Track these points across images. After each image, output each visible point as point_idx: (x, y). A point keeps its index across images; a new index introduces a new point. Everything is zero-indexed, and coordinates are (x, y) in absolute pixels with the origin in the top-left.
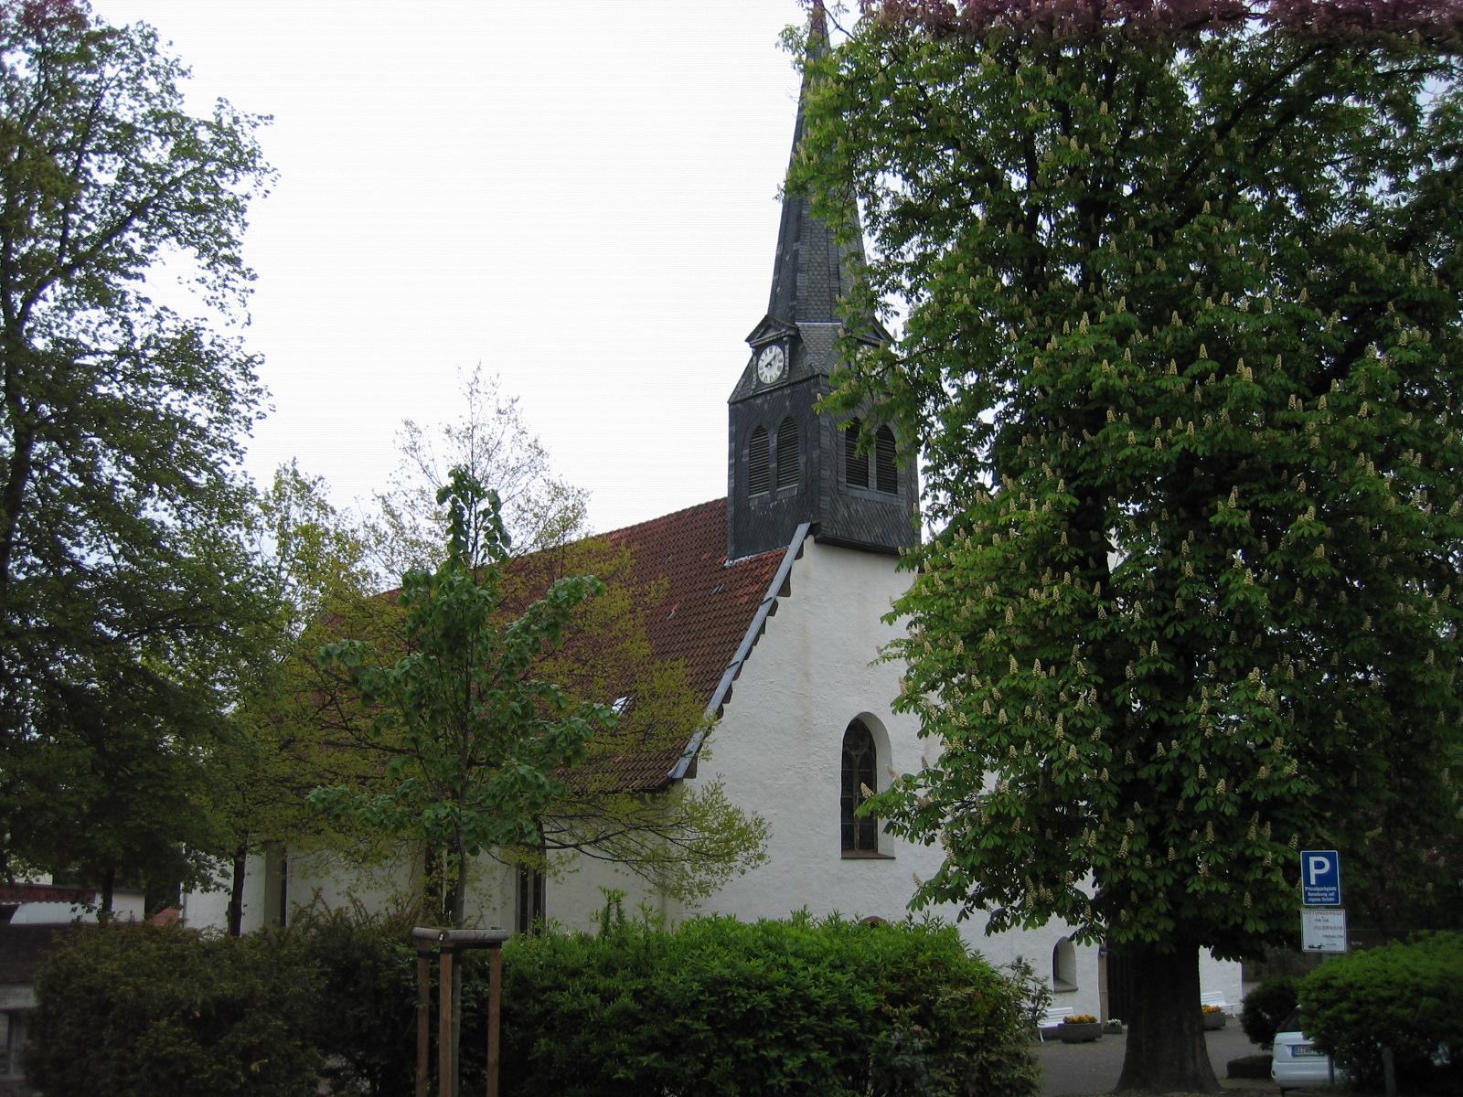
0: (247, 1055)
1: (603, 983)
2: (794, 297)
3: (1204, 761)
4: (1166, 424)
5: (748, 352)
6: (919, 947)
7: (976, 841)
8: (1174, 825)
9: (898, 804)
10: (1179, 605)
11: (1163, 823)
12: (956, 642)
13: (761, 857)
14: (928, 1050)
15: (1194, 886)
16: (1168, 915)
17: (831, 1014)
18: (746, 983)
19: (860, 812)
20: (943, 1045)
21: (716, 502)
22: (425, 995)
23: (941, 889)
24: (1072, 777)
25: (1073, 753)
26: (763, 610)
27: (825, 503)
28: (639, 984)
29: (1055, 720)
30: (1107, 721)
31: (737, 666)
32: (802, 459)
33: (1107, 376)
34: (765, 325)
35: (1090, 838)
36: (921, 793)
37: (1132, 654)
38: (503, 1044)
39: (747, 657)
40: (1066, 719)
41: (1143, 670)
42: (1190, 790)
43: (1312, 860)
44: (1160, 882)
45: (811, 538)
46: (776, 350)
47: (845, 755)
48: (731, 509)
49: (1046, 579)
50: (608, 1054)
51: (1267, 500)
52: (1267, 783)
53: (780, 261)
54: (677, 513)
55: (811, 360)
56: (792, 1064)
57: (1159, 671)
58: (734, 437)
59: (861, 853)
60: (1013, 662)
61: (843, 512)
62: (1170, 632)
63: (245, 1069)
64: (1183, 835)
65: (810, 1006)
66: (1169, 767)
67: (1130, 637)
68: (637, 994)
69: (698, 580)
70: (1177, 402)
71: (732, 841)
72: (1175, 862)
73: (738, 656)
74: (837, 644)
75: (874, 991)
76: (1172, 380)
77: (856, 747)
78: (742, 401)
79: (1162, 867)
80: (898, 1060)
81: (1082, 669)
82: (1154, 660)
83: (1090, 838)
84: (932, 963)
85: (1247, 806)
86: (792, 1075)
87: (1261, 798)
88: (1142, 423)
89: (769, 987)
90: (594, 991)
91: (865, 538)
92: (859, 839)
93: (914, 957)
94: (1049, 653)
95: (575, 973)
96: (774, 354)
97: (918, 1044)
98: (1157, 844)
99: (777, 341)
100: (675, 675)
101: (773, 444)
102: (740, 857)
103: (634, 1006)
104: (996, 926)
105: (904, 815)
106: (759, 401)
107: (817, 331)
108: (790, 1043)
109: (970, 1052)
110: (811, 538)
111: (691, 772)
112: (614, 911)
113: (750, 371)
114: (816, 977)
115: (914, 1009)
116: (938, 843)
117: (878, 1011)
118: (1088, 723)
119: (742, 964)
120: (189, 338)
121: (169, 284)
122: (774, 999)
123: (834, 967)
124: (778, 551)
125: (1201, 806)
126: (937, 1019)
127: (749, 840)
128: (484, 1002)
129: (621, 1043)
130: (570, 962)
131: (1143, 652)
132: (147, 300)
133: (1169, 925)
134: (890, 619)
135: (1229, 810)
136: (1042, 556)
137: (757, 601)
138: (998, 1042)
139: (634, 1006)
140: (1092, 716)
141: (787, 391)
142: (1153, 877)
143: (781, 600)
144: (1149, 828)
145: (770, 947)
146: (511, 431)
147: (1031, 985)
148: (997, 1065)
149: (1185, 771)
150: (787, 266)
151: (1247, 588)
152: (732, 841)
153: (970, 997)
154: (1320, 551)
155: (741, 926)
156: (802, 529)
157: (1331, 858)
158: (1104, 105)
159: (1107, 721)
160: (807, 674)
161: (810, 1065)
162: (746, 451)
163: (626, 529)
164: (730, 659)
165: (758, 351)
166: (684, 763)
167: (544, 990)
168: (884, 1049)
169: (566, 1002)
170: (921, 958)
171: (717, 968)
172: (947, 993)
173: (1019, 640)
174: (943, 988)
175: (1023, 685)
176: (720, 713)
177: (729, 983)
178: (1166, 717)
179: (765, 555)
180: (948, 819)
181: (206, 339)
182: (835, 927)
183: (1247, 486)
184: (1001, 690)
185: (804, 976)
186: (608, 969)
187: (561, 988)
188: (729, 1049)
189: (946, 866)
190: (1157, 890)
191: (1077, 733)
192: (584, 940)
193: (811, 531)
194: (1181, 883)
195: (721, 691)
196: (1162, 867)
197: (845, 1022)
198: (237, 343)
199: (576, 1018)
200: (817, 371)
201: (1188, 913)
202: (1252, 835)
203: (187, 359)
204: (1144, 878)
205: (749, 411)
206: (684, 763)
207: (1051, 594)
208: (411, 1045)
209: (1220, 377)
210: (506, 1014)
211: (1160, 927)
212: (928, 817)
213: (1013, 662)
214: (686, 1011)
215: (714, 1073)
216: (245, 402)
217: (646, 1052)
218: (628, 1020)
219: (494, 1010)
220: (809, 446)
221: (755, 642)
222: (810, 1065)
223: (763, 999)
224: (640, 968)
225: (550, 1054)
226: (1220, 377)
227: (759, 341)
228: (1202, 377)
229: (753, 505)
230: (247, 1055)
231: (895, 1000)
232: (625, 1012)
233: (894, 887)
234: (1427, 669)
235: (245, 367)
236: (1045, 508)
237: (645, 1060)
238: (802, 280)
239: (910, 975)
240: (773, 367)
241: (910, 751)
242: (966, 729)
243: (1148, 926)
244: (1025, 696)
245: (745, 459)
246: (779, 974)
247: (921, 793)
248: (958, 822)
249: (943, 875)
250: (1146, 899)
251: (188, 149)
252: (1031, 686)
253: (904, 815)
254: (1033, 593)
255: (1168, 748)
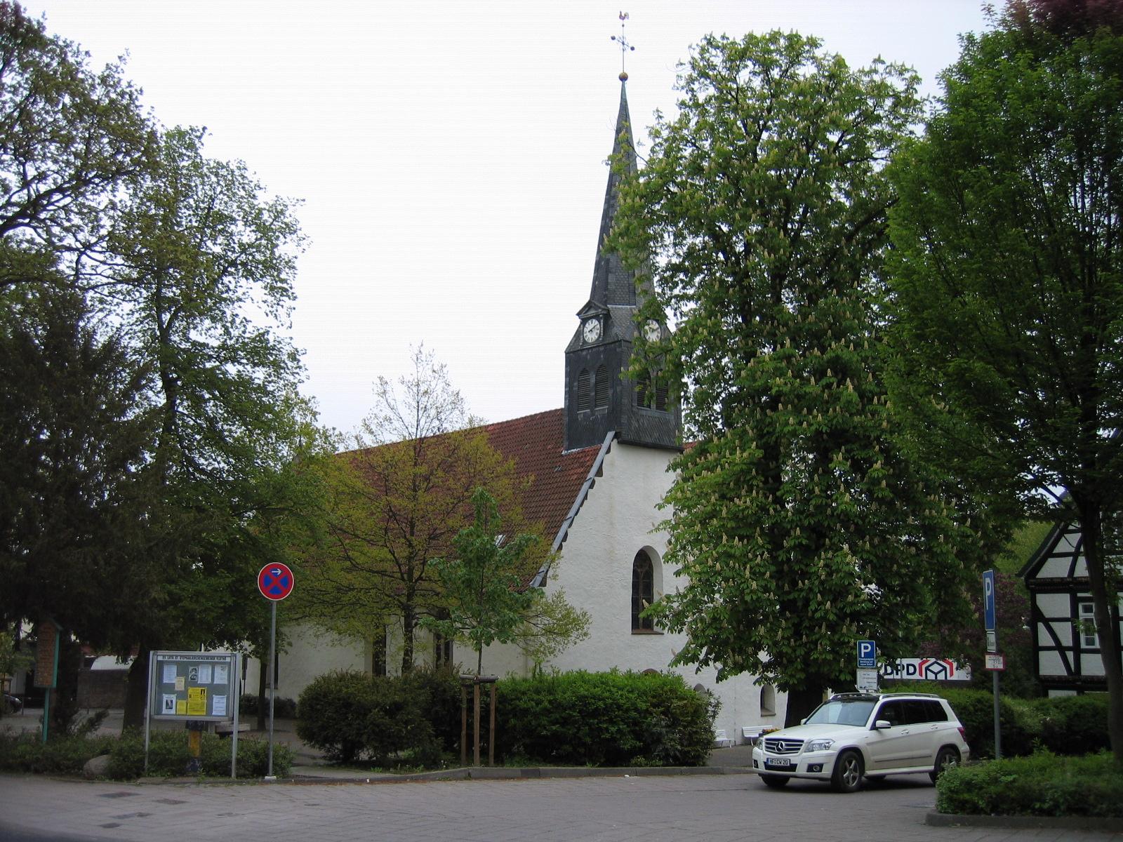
0: (406, 723)
1: (536, 697)
2: (606, 289)
3: (820, 592)
4: (810, 412)
5: (578, 321)
6: (665, 684)
7: (703, 631)
8: (806, 623)
9: (662, 611)
10: (811, 508)
11: (800, 624)
12: (699, 523)
13: (586, 634)
14: (667, 726)
15: (814, 656)
16: (802, 670)
17: (627, 710)
18: (594, 698)
19: (642, 615)
20: (674, 723)
21: (556, 410)
22: (465, 702)
23: (686, 657)
24: (755, 597)
25: (754, 584)
26: (586, 485)
27: (624, 419)
28: (551, 698)
29: (745, 569)
30: (773, 568)
31: (569, 521)
32: (610, 392)
33: (779, 386)
34: (588, 306)
35: (762, 630)
36: (675, 605)
37: (787, 533)
38: (496, 720)
39: (576, 514)
40: (751, 568)
41: (792, 543)
42: (813, 606)
43: (863, 645)
44: (798, 653)
45: (615, 441)
46: (595, 322)
47: (634, 571)
48: (566, 419)
49: (743, 492)
50: (539, 725)
51: (860, 454)
52: (852, 604)
53: (598, 264)
54: (531, 416)
55: (618, 331)
56: (613, 729)
57: (800, 544)
58: (568, 374)
59: (644, 631)
60: (725, 537)
61: (635, 424)
62: (806, 523)
63: (406, 728)
64: (811, 629)
65: (619, 707)
66: (804, 594)
67: (785, 525)
68: (550, 702)
69: (544, 461)
70: (815, 399)
71: (568, 625)
72: (806, 643)
73: (571, 514)
74: (632, 501)
75: (645, 702)
76: (813, 387)
77: (641, 566)
78: (574, 352)
79: (800, 646)
80: (654, 730)
81: (760, 541)
82: (798, 538)
83: (762, 630)
84: (670, 690)
85: (842, 616)
86: (612, 734)
87: (848, 612)
88: (797, 411)
89: (603, 699)
90: (533, 700)
91: (649, 440)
92: (642, 624)
93: (662, 689)
94: (743, 532)
95: (524, 693)
96: (593, 324)
97: (663, 723)
98: (797, 634)
99: (596, 317)
100: (534, 531)
101: (593, 380)
102: (574, 634)
103: (549, 706)
104: (721, 678)
105: (666, 616)
106: (584, 353)
107: (620, 310)
108: (611, 721)
109: (685, 727)
110: (615, 441)
111: (543, 584)
112: (538, 670)
113: (579, 334)
114: (621, 696)
115: (662, 709)
116: (684, 633)
117: (647, 710)
118: (762, 570)
119: (592, 690)
120: (261, 337)
121: (250, 306)
122: (605, 704)
123: (629, 692)
124: (594, 447)
125: (818, 615)
126: (672, 714)
127: (578, 624)
128: (488, 705)
129: (544, 720)
130: (522, 689)
131: (792, 533)
132: (237, 315)
133: (802, 676)
134: (660, 507)
135: (831, 617)
136: (741, 480)
137: (582, 478)
138: (696, 724)
139: (549, 706)
140: (765, 566)
141: (602, 349)
142: (795, 651)
143: (597, 479)
144: (794, 625)
145: (603, 683)
146: (441, 385)
147: (712, 700)
148: (696, 732)
149: (811, 596)
150: (602, 268)
151: (846, 503)
152: (568, 625)
153: (685, 705)
154: (884, 483)
155: (589, 675)
156: (610, 435)
157: (871, 644)
158: (782, 233)
159: (773, 568)
160: (612, 524)
161: (619, 731)
162: (576, 384)
163: (498, 424)
164: (566, 514)
165: (584, 322)
166: (539, 578)
167: (512, 700)
168: (649, 725)
169: (522, 704)
170: (665, 689)
171: (582, 691)
172: (676, 703)
173: (730, 524)
174: (675, 701)
175: (729, 550)
176: (560, 547)
177: (587, 697)
178: (803, 567)
179: (587, 449)
180: (689, 619)
181: (271, 337)
182: (629, 675)
183: (849, 447)
184: (717, 553)
185: (617, 695)
186: (538, 692)
187: (519, 699)
188: (587, 724)
189: (689, 644)
190: (797, 657)
191: (756, 575)
192: (525, 680)
193: (616, 436)
194: (808, 654)
195: (561, 534)
196: (800, 646)
197: (633, 714)
198: (289, 341)
199: (526, 712)
200: (620, 338)
201: (812, 670)
202: (844, 630)
203: (260, 350)
204: (790, 651)
205: (577, 358)
206: (539, 578)
207: (744, 502)
208: (459, 722)
209: (838, 386)
210: (497, 709)
211: (798, 676)
212: (678, 621)
213: (725, 537)
214: (570, 708)
215: (581, 733)
216: (293, 374)
217: (554, 725)
218: (547, 712)
219: (493, 707)
220: (612, 384)
221: (581, 505)
222: (619, 731)
223: (601, 704)
224: (551, 691)
225: (515, 725)
226: (838, 386)
227: (585, 315)
228: (829, 386)
229: (580, 417)
230: (406, 723)
231: (654, 706)
232: (546, 709)
233: (660, 653)
234: (940, 544)
235: (293, 357)
236: (745, 455)
237: (554, 728)
238: (611, 278)
239: (660, 695)
240: (593, 332)
241: (671, 582)
242: (700, 573)
243: (792, 676)
244: (730, 556)
245: (575, 389)
246: (607, 694)
247: (675, 605)
248: (695, 621)
249: (686, 649)
250: (791, 662)
251: (263, 230)
252: (733, 551)
253: (666, 616)
254: (736, 500)
255: (804, 584)
